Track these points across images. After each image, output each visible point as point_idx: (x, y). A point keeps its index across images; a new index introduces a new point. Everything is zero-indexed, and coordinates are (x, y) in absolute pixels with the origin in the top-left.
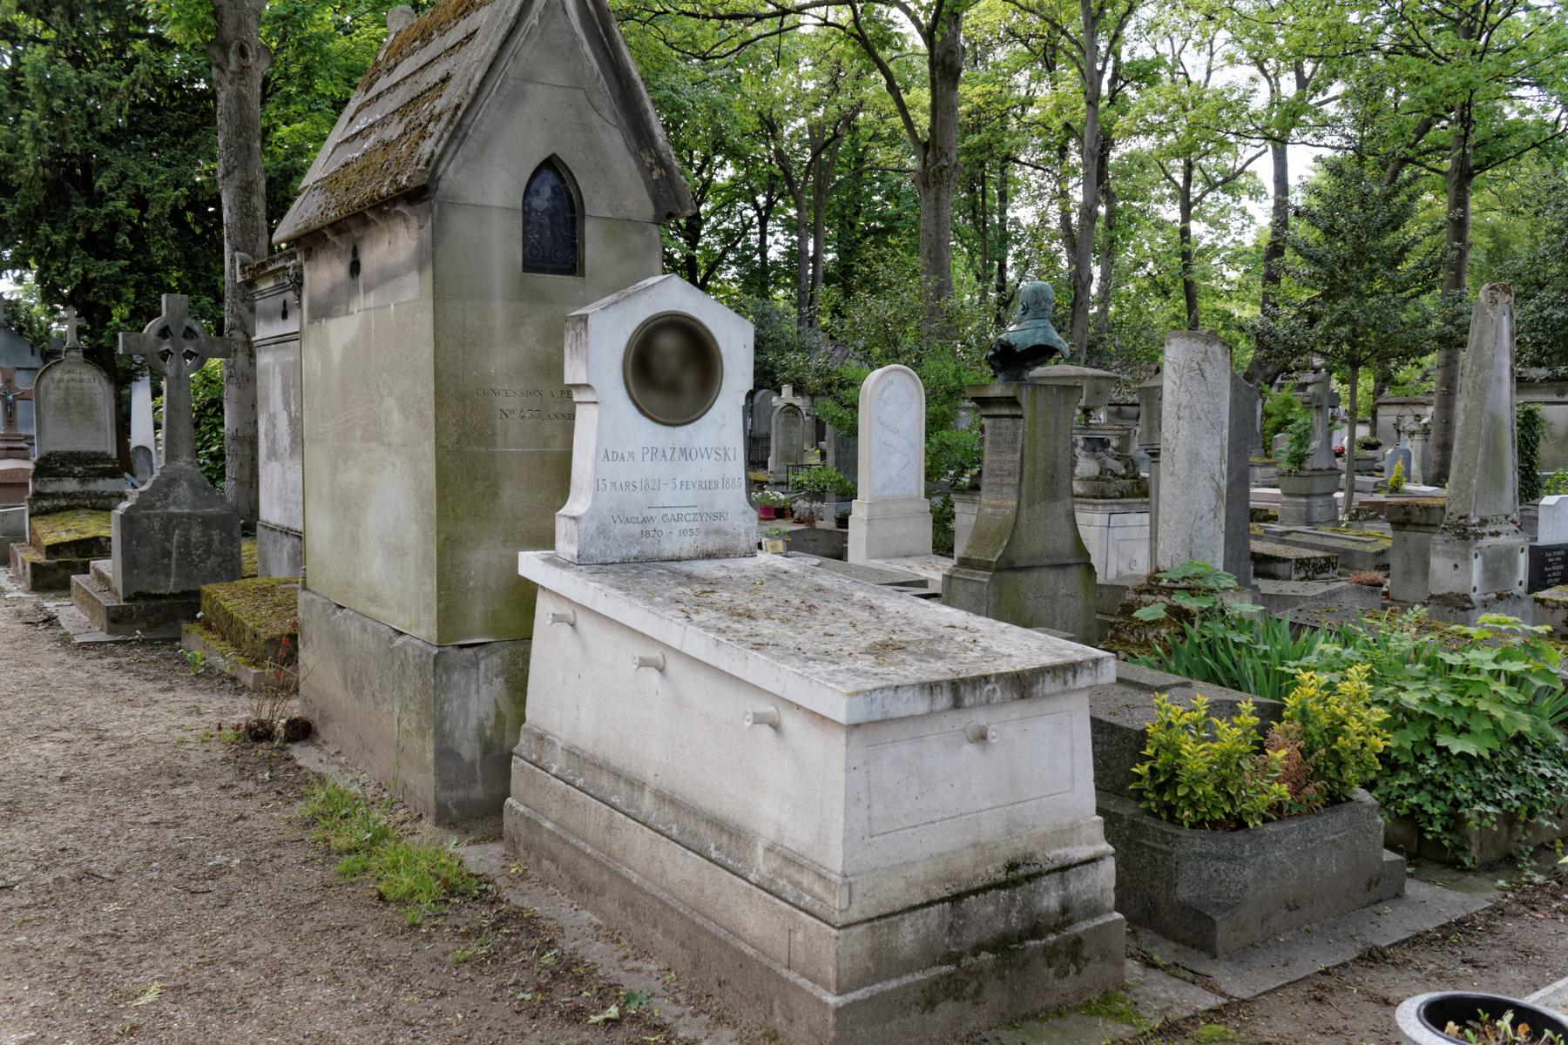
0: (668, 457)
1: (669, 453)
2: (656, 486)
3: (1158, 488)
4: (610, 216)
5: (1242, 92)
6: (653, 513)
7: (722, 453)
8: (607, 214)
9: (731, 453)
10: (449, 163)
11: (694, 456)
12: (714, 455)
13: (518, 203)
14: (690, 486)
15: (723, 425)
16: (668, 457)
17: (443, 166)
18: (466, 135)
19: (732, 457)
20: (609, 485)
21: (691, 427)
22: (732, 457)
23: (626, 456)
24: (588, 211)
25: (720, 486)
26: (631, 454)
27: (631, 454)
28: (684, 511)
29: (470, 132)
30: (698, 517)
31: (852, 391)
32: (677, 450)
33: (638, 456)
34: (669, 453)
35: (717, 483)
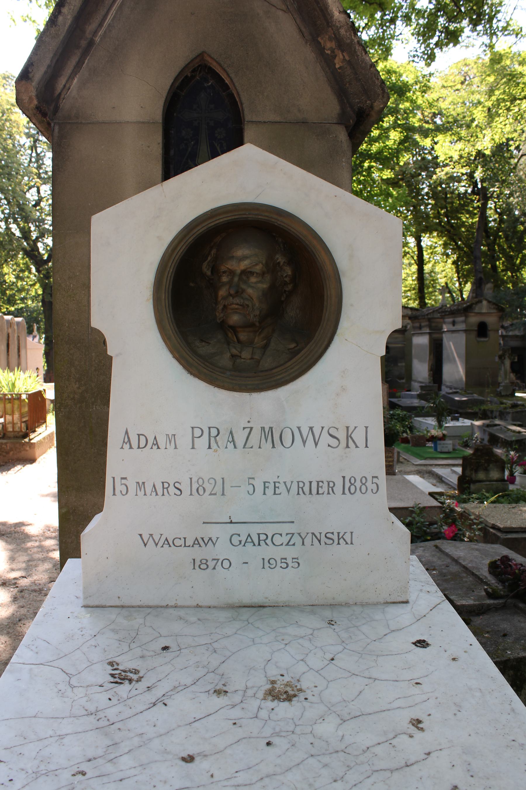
0: (240, 442)
1: (240, 437)
2: (218, 489)
3: (240, 98)
4: (278, 119)
5: (484, 525)
6: (213, 531)
7: (342, 436)
8: (272, 117)
9: (359, 436)
10: (71, 78)
11: (288, 441)
12: (325, 439)
13: (158, 115)
14: (282, 489)
15: (343, 389)
16: (240, 442)
17: (62, 81)
18: (91, 43)
19: (361, 442)
20: (132, 487)
21: (283, 392)
22: (361, 442)
23: (162, 441)
24: (248, 116)
25: (338, 488)
26: (172, 438)
27: (172, 438)
28: (270, 530)
29: (97, 39)
30: (297, 539)
31: (402, 364)
32: (256, 434)
33: (184, 441)
34: (240, 437)
35: (331, 488)
